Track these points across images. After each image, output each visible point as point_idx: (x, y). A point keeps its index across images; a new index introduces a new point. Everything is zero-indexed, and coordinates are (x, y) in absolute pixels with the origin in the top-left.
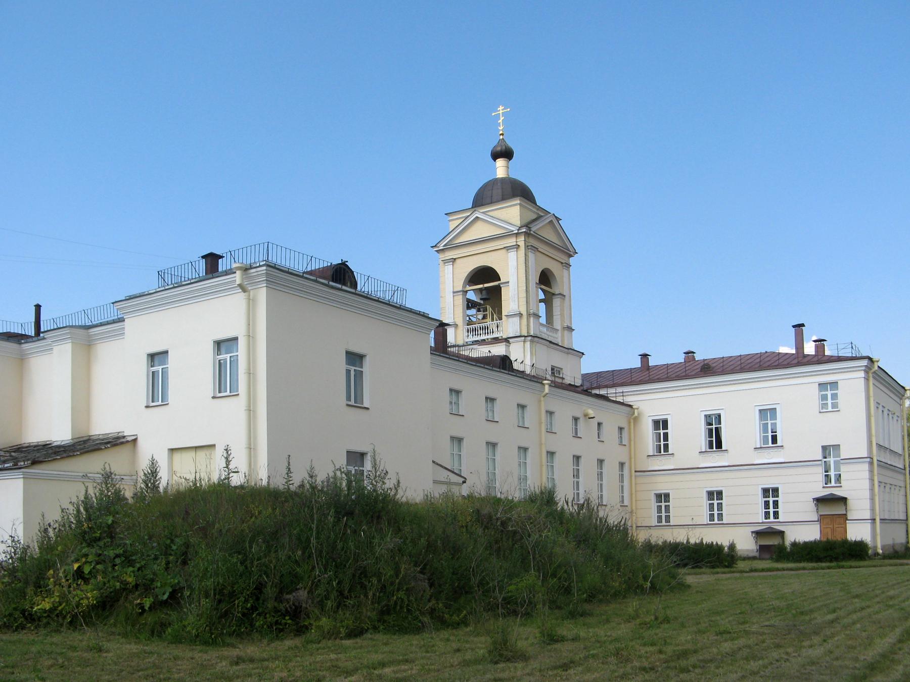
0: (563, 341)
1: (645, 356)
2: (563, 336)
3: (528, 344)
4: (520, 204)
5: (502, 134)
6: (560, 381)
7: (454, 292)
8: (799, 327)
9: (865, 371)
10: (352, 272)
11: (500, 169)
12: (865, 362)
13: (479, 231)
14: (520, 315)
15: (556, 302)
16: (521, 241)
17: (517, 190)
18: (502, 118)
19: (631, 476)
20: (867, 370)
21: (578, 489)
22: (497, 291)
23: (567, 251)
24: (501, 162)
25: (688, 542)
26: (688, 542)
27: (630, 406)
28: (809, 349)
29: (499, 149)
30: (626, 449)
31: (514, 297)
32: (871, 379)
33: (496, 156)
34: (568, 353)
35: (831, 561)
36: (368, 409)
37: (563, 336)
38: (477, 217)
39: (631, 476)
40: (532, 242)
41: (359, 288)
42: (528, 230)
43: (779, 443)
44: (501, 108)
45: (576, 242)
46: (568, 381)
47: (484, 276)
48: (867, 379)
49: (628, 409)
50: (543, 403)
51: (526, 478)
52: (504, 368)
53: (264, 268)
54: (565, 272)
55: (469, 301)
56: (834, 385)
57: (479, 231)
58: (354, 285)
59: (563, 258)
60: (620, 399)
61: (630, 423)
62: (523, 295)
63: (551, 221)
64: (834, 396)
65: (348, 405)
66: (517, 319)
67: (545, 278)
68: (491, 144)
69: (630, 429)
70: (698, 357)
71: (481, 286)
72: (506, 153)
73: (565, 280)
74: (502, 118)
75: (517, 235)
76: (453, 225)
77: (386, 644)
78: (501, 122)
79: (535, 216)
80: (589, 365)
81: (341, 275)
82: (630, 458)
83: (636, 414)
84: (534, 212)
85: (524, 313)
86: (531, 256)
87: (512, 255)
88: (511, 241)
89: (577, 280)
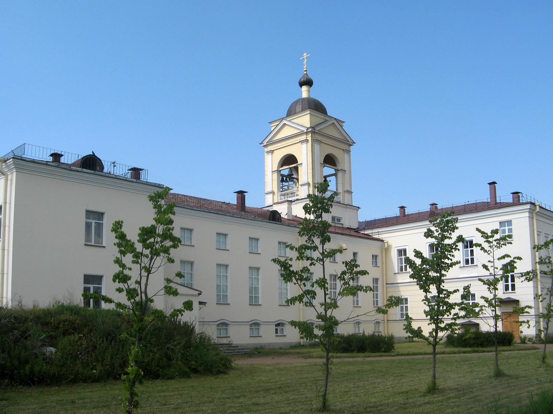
0: (344, 200)
1: (402, 208)
2: (344, 197)
4: (310, 113)
5: (306, 71)
6: (341, 226)
7: (272, 172)
8: (493, 184)
9: (529, 212)
10: (100, 160)
11: (304, 92)
12: (528, 206)
13: (287, 132)
15: (340, 175)
16: (309, 137)
17: (316, 107)
18: (306, 61)
19: (383, 287)
20: (531, 211)
21: (377, 298)
22: (296, 169)
23: (347, 143)
24: (304, 88)
25: (364, 333)
26: (364, 333)
27: (382, 241)
28: (504, 196)
29: (302, 80)
30: (380, 269)
32: (535, 218)
33: (301, 84)
34: (346, 208)
35: (477, 347)
36: (104, 247)
37: (344, 197)
38: (285, 124)
39: (383, 287)
40: (317, 137)
41: (105, 170)
42: (313, 130)
43: (475, 264)
44: (305, 54)
45: (353, 135)
46: (346, 225)
47: (289, 160)
48: (531, 218)
49: (380, 243)
50: (300, 240)
51: (257, 289)
52: (273, 220)
53: (11, 160)
54: (346, 156)
55: (283, 176)
56: (509, 222)
57: (287, 132)
58: (102, 168)
60: (376, 236)
61: (382, 252)
62: (310, 171)
63: (333, 123)
65: (86, 245)
66: (306, 187)
68: (299, 77)
69: (382, 257)
70: (439, 207)
71: (288, 167)
72: (308, 83)
73: (346, 160)
74: (306, 61)
75: (307, 133)
76: (273, 128)
77: (264, 397)
78: (305, 65)
79: (324, 121)
80: (364, 216)
81: (91, 163)
82: (383, 275)
83: (386, 246)
84: (322, 118)
85: (311, 183)
86: (317, 146)
87: (304, 145)
88: (303, 137)
89: (357, 161)
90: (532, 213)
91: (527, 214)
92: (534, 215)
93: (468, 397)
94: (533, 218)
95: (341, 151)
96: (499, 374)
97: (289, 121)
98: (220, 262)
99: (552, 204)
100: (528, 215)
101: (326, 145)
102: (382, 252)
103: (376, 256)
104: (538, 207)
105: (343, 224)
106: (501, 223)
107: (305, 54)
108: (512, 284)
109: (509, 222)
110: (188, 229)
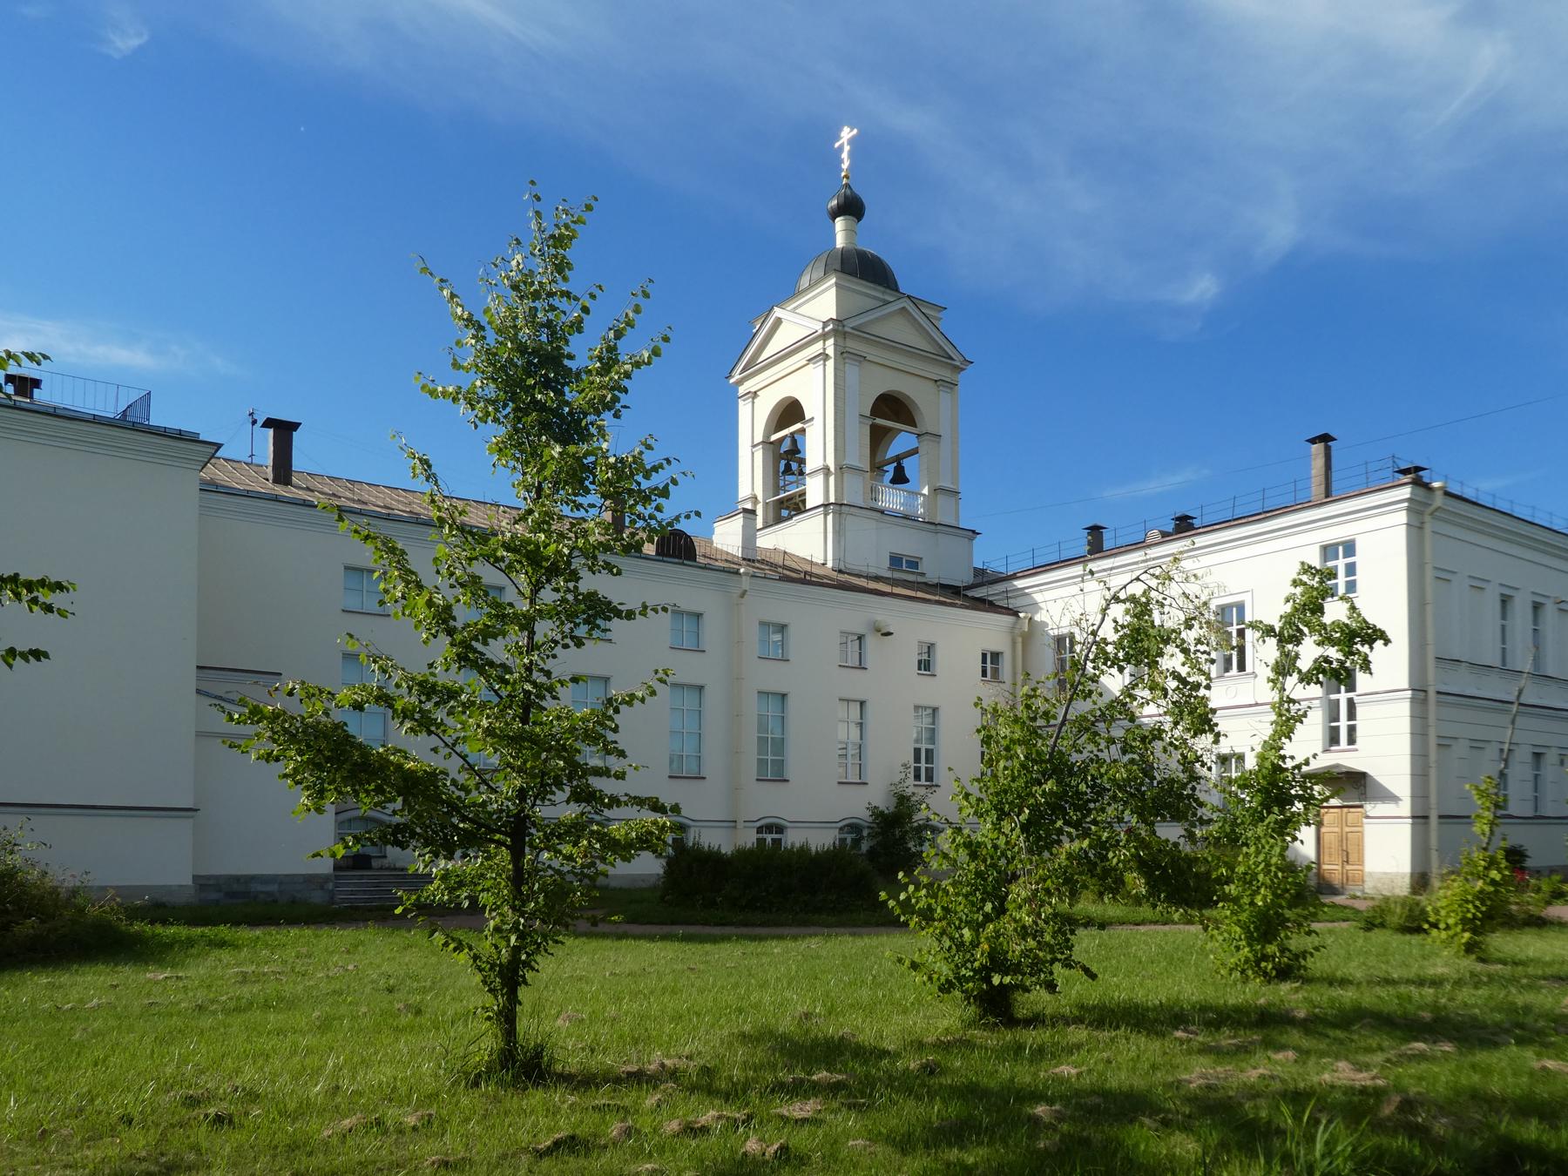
3: (830, 517)
6: (920, 579)
14: (826, 470)
24: (840, 223)
31: (819, 447)
32: (1428, 528)
33: (835, 214)
40: (852, 345)
46: (932, 576)
48: (1416, 529)
54: (945, 397)
59: (946, 374)
64: (1351, 570)
67: (892, 410)
72: (851, 207)
75: (824, 337)
86: (852, 371)
88: (817, 348)
90: (1421, 513)
91: (1402, 517)
92: (1427, 518)
93: (1337, 992)
94: (1421, 528)
95: (931, 384)
96: (524, 1067)
97: (794, 311)
98: (765, 689)
99: (1565, 508)
100: (1404, 520)
101: (902, 375)
102: (1014, 643)
103: (996, 656)
104: (1439, 494)
105: (923, 574)
106: (1328, 551)
107: (846, 129)
108: (1337, 720)
109: (1350, 548)
110: (690, 614)
